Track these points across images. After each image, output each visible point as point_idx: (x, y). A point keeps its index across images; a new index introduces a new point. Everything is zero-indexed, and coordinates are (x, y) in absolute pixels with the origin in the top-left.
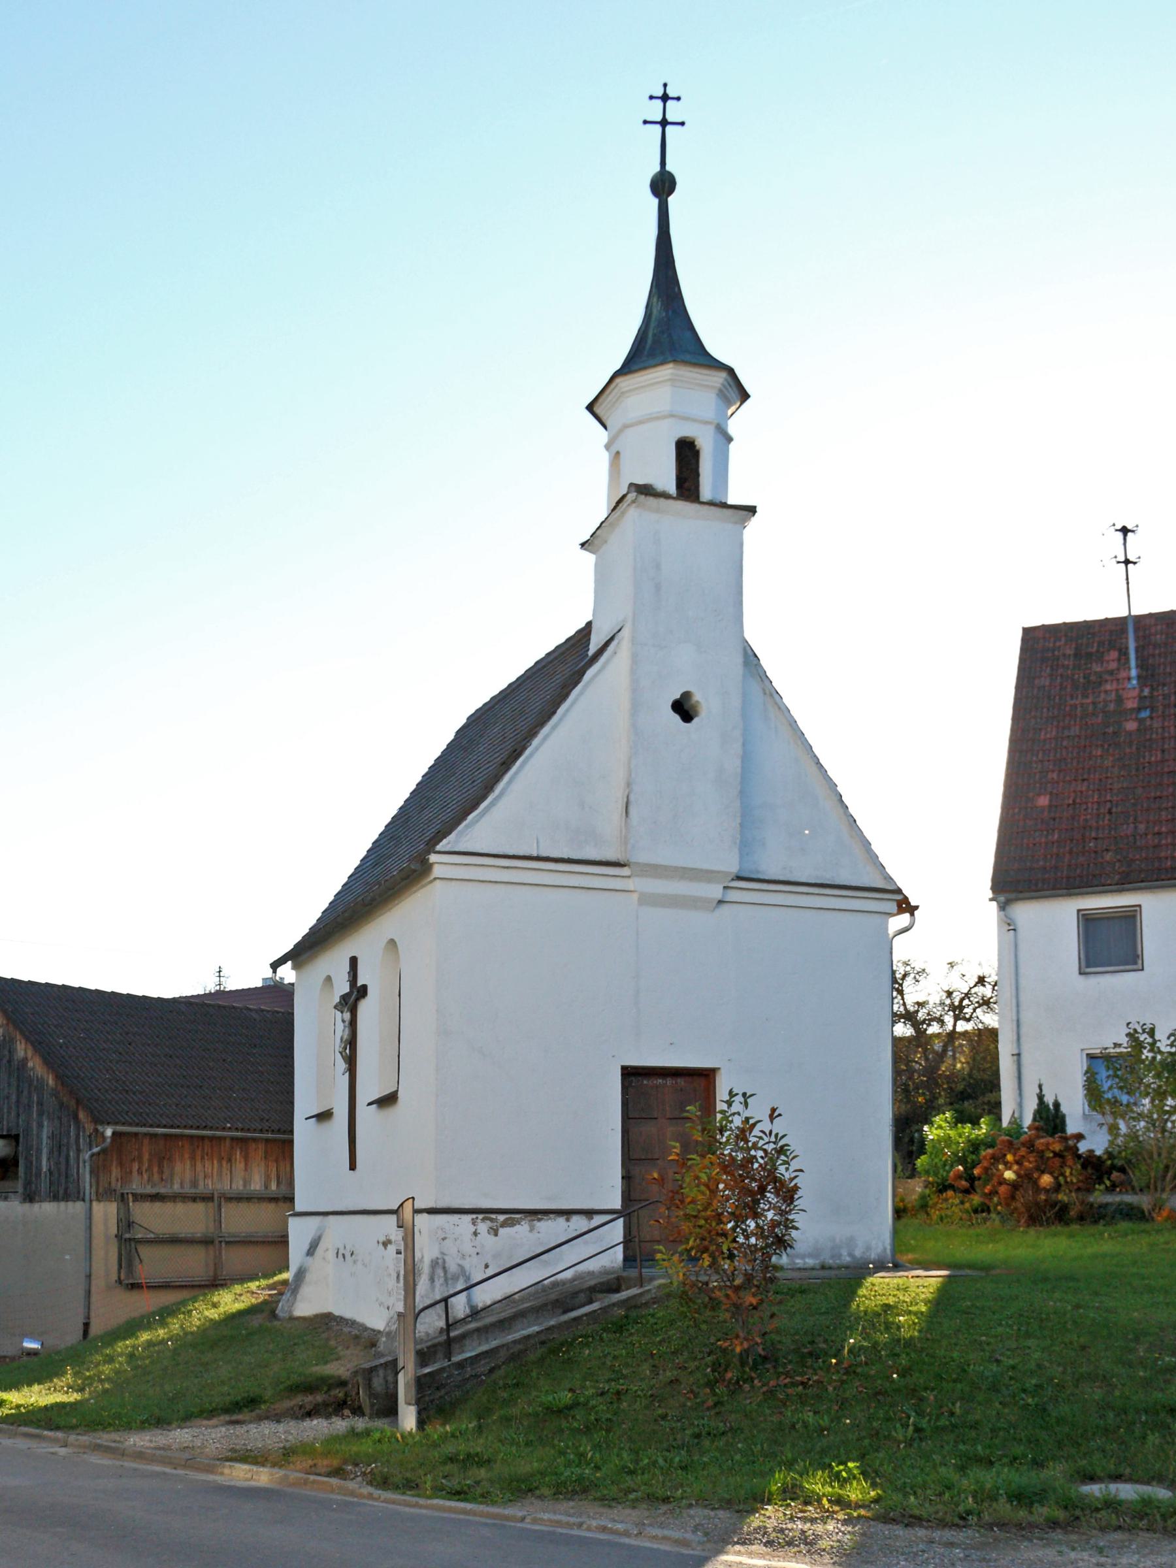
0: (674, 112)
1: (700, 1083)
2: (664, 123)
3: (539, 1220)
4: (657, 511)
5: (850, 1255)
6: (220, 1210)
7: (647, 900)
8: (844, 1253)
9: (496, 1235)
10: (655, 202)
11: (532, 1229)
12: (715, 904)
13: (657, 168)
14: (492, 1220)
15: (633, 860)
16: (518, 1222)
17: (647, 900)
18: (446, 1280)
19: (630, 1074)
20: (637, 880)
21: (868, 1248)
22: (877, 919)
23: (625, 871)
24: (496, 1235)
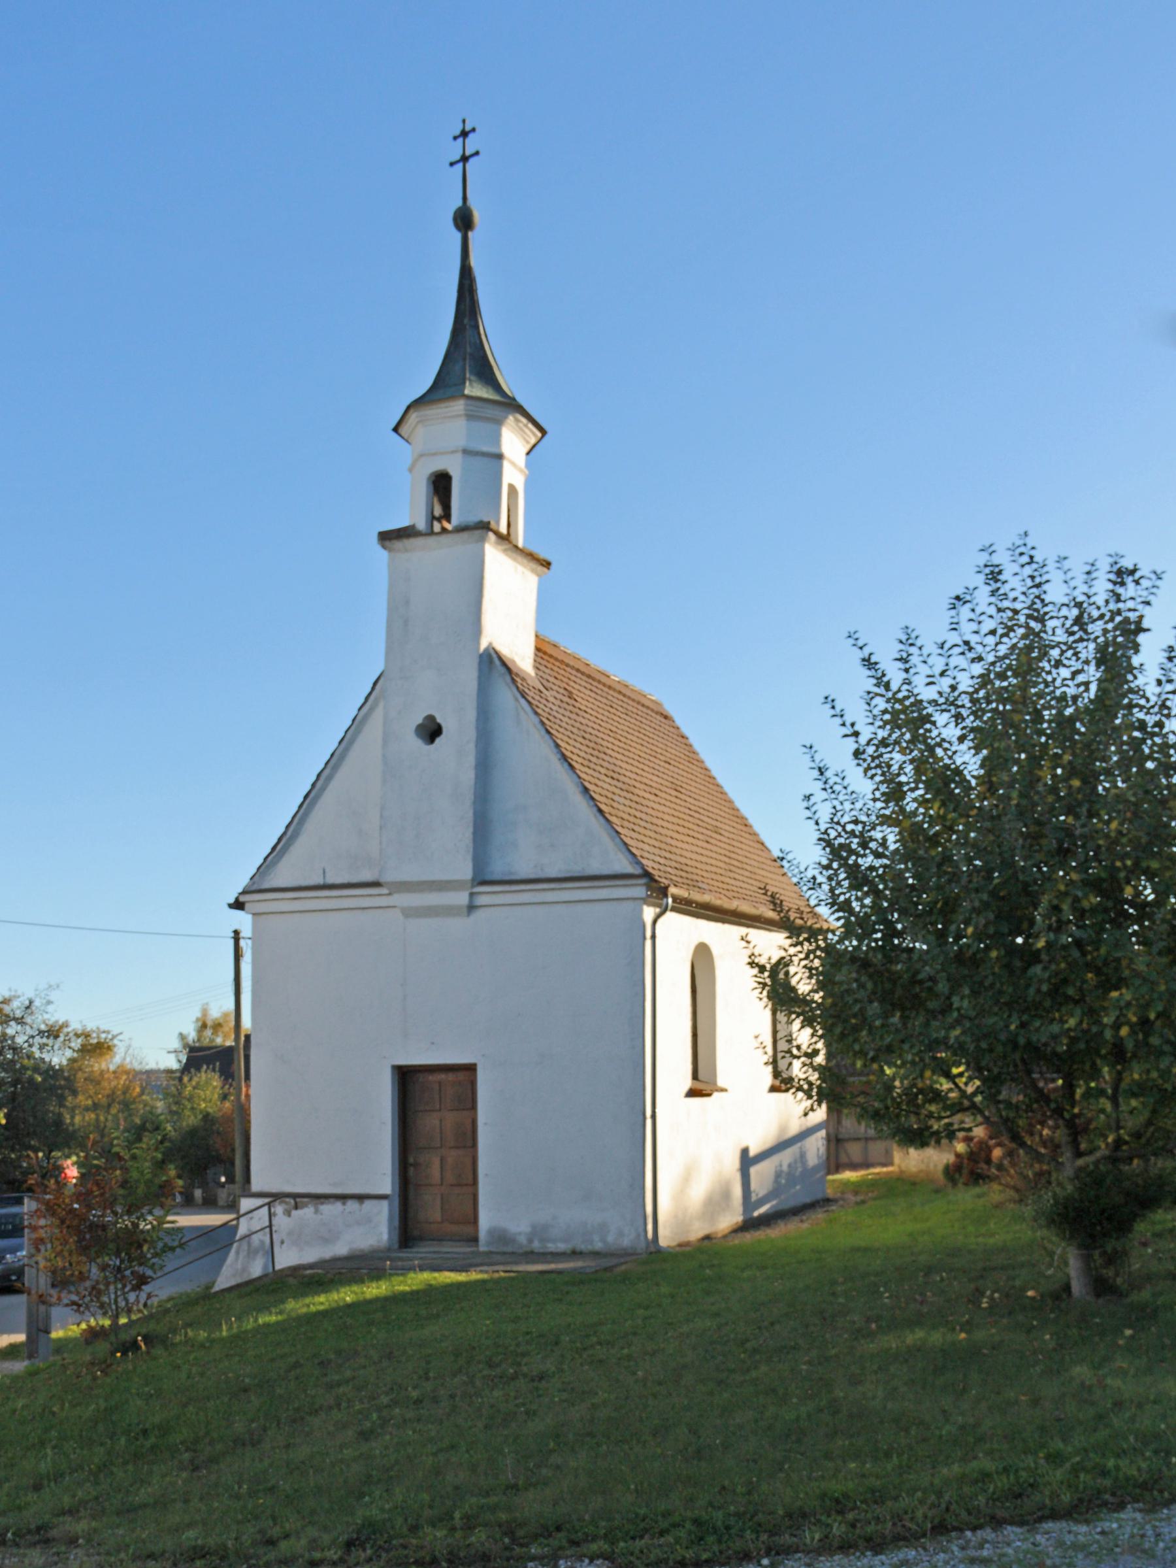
0: (472, 144)
1: (461, 1076)
2: (465, 159)
3: (322, 1203)
4: (406, 551)
5: (603, 1240)
6: (442, 1179)
7: (410, 913)
8: (596, 1238)
9: (289, 1215)
10: (458, 236)
11: (316, 1211)
12: (465, 910)
13: (460, 203)
14: (286, 1203)
15: (382, 880)
16: (305, 1205)
17: (410, 913)
18: (249, 1253)
19: (470, 1069)
20: (396, 896)
21: (621, 1234)
22: (630, 905)
23: (384, 891)
24: (289, 1215)
